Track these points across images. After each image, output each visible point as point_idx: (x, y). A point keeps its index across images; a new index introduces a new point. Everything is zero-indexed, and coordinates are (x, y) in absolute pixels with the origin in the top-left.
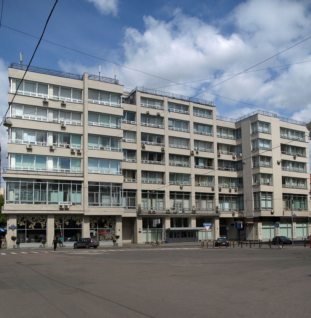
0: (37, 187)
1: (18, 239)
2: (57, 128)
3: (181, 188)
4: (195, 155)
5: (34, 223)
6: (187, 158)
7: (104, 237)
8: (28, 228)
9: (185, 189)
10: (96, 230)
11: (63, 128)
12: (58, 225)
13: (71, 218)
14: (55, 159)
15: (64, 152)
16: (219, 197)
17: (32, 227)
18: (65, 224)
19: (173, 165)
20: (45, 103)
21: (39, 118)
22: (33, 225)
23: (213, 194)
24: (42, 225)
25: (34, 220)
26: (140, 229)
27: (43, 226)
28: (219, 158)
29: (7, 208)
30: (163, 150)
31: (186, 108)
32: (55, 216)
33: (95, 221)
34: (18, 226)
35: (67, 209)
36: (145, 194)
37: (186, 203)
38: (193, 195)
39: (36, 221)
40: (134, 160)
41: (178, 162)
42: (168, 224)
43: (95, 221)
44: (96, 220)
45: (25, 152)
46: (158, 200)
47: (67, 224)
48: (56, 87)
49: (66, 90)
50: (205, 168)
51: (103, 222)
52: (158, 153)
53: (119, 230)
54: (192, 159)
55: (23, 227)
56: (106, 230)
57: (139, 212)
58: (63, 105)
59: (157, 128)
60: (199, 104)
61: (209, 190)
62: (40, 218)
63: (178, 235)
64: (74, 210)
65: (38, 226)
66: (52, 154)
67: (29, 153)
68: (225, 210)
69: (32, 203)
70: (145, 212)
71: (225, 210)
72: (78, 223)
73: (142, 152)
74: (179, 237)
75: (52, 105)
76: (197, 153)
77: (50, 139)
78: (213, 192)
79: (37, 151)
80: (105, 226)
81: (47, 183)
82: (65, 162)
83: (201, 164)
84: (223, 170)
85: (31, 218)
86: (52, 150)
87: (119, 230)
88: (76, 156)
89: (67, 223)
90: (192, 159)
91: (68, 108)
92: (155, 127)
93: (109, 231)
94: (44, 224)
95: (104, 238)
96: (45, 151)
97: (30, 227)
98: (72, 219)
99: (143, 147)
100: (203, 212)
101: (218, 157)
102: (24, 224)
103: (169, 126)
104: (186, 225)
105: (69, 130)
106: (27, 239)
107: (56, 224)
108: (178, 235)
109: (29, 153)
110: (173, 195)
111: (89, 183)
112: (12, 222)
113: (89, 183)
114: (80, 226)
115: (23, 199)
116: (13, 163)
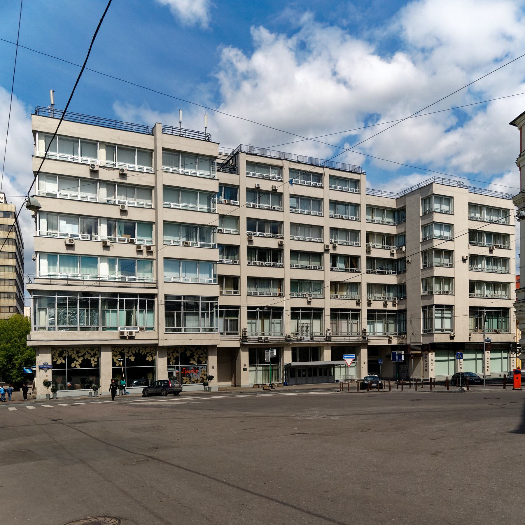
0: (84, 304)
1: (54, 385)
2: (114, 213)
3: (309, 303)
4: (332, 251)
5: (80, 360)
6: (318, 256)
7: (190, 378)
8: (69, 366)
9: (316, 304)
10: (177, 368)
11: (124, 212)
12: (117, 362)
13: (139, 351)
14: (111, 260)
15: (124, 250)
16: (368, 315)
17: (76, 365)
18: (129, 360)
19: (297, 267)
20: (94, 172)
21: (84, 196)
22: (78, 363)
23: (359, 310)
24: (92, 362)
25: (80, 355)
26: (245, 366)
27: (93, 364)
28: (368, 255)
29: (36, 337)
30: (281, 245)
31: (319, 177)
32: (113, 348)
33: (176, 355)
34: (54, 365)
35: (132, 337)
36: (253, 312)
37: (316, 325)
38: (327, 313)
39: (83, 356)
40: (236, 260)
41: (304, 263)
42: (287, 357)
43: (176, 355)
44: (178, 352)
45: (63, 250)
46: (273, 321)
47: (133, 360)
48: (110, 147)
49: (127, 151)
50: (346, 271)
51: (188, 355)
52: (273, 250)
53: (213, 368)
54: (327, 258)
55: (62, 365)
56: (192, 368)
57: (244, 338)
58: (123, 175)
59: (272, 210)
60: (338, 171)
61: (351, 305)
62: (90, 351)
63: (304, 373)
64: (142, 338)
65: (86, 363)
66: (106, 253)
67: (70, 252)
68: (378, 334)
69: (76, 329)
70: (253, 340)
71: (378, 334)
72: (149, 359)
73: (249, 248)
74: (304, 376)
75: (104, 175)
76: (334, 248)
77: (103, 230)
78: (358, 307)
79: (83, 247)
80: (191, 362)
81: (100, 298)
82: (127, 266)
83: (340, 265)
84: (375, 273)
85: (75, 352)
86: (106, 247)
87: (213, 368)
88: (145, 255)
89: (132, 359)
90: (327, 258)
91: (132, 179)
92: (269, 210)
93: (198, 369)
94: (96, 360)
95: (190, 380)
96: (96, 249)
97: (73, 365)
98: (141, 352)
99: (250, 241)
100: (342, 338)
101: (367, 254)
102: (63, 362)
103: (291, 207)
104: (316, 358)
105: (133, 215)
106: (68, 384)
107: (115, 360)
108: (304, 373)
109: (70, 252)
110: (296, 313)
111: (166, 297)
112: (44, 358)
113: (166, 297)
114: (153, 362)
115: (61, 323)
116: (44, 268)
